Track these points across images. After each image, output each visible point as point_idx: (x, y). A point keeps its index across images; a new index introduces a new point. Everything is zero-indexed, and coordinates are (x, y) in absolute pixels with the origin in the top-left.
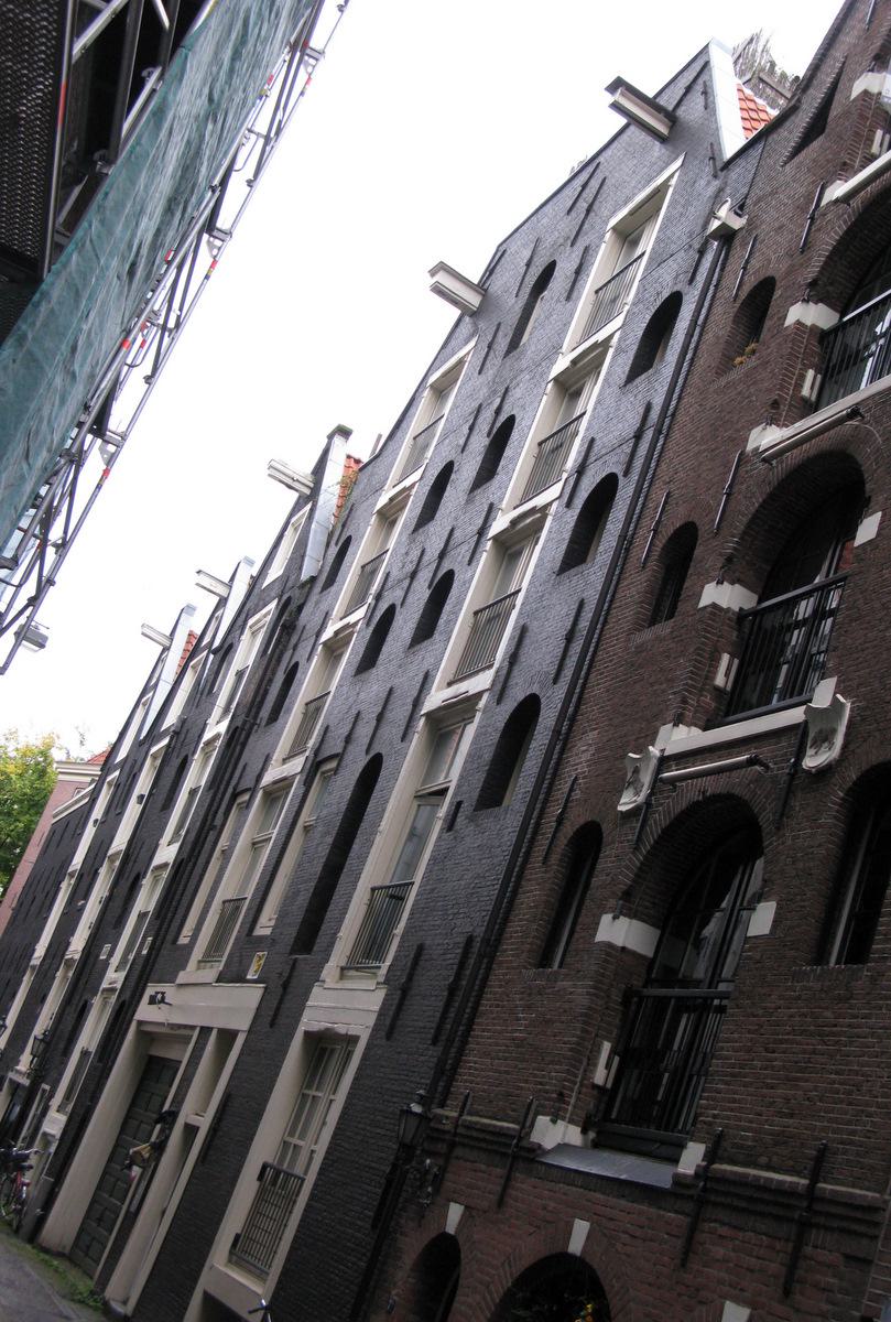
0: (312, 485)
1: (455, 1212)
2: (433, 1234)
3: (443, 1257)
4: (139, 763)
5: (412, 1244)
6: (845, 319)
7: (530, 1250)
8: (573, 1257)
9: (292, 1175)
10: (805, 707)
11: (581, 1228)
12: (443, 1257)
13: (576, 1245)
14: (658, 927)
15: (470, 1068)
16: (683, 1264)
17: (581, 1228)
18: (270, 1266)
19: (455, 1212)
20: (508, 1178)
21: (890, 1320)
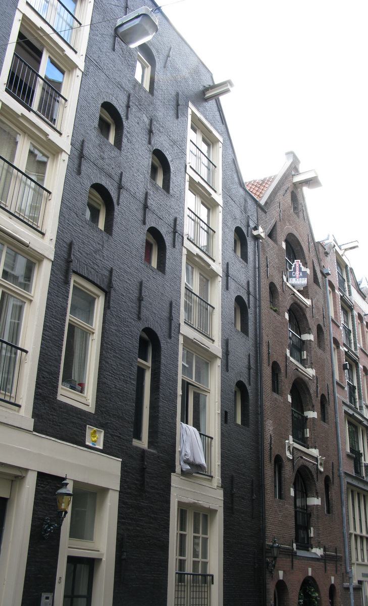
0: (137, 313)
1: (281, 573)
2: (276, 581)
3: (281, 586)
4: (336, 464)
5: (271, 587)
6: (348, 368)
7: (301, 578)
8: (310, 576)
9: (185, 574)
10: (220, 355)
11: (310, 570)
12: (281, 586)
13: (310, 574)
14: (310, 506)
15: (269, 528)
16: (325, 572)
17: (310, 570)
18: (176, 559)
19: (281, 573)
20: (292, 561)
21: (367, 605)
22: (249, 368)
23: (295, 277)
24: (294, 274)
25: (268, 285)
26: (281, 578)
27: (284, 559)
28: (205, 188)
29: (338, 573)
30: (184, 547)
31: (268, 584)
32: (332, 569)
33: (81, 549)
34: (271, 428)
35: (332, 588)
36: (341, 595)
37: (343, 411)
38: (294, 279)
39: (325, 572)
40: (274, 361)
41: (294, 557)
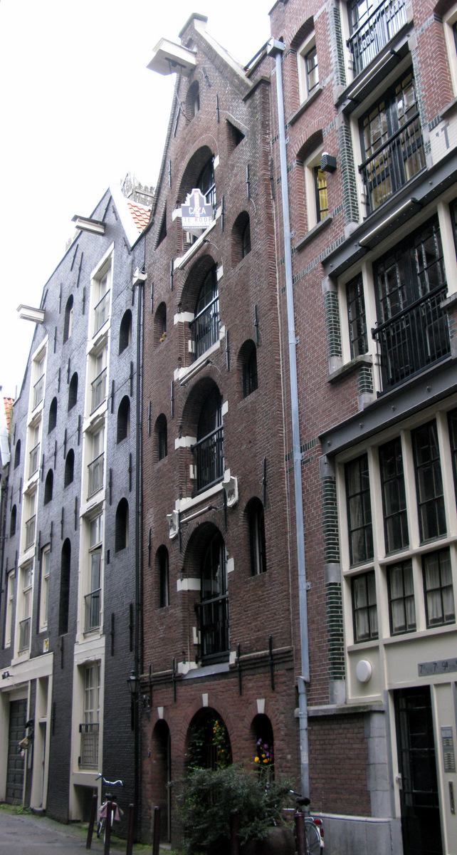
1: (161, 710)
3: (162, 729)
5: (149, 729)
11: (205, 697)
13: (205, 703)
17: (205, 697)
19: (161, 710)
22: (130, 471)
23: (193, 216)
24: (192, 211)
25: (124, 311)
26: (161, 717)
27: (165, 690)
28: (68, 331)
29: (277, 689)
30: (275, 330)
31: (145, 727)
32: (260, 684)
33: (43, 720)
34: (151, 520)
35: (262, 726)
36: (286, 735)
37: (160, 464)
38: (192, 219)
39: (241, 694)
40: (163, 414)
41: (178, 683)
